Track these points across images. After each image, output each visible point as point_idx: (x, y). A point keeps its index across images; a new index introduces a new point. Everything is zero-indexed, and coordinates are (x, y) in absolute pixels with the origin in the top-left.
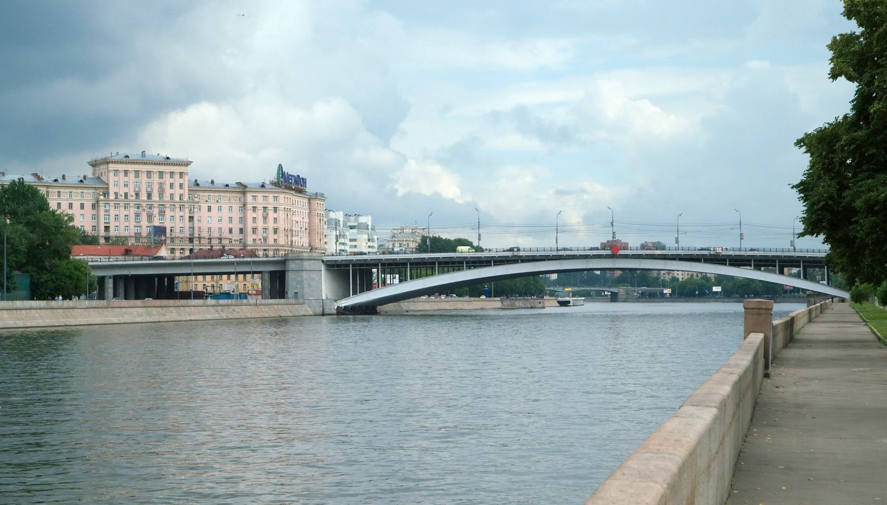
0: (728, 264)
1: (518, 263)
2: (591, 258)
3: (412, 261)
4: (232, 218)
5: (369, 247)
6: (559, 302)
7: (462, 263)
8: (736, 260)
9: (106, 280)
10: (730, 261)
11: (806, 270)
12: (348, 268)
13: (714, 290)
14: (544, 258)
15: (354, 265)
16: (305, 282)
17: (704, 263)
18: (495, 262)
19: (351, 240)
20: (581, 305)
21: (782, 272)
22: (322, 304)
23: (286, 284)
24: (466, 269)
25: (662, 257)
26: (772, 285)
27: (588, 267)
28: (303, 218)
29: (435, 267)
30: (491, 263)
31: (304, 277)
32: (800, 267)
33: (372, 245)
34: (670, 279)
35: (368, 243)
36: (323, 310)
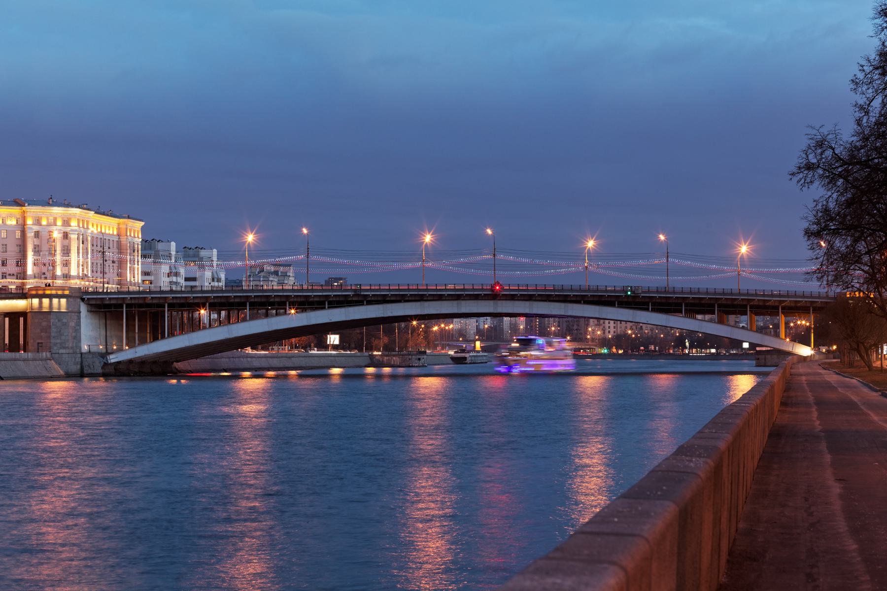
0: (650, 309)
1: (363, 305)
2: (482, 299)
4: (6, 245)
8: (661, 304)
10: (654, 304)
11: (3, 222)
13: (337, 337)
14: (398, 299)
15: (128, 306)
16: (53, 329)
17: (618, 307)
20: (482, 363)
21: (721, 321)
22: (80, 360)
25: (561, 299)
30: (325, 305)
31: (52, 321)
32: (714, 314)
35: (212, 284)
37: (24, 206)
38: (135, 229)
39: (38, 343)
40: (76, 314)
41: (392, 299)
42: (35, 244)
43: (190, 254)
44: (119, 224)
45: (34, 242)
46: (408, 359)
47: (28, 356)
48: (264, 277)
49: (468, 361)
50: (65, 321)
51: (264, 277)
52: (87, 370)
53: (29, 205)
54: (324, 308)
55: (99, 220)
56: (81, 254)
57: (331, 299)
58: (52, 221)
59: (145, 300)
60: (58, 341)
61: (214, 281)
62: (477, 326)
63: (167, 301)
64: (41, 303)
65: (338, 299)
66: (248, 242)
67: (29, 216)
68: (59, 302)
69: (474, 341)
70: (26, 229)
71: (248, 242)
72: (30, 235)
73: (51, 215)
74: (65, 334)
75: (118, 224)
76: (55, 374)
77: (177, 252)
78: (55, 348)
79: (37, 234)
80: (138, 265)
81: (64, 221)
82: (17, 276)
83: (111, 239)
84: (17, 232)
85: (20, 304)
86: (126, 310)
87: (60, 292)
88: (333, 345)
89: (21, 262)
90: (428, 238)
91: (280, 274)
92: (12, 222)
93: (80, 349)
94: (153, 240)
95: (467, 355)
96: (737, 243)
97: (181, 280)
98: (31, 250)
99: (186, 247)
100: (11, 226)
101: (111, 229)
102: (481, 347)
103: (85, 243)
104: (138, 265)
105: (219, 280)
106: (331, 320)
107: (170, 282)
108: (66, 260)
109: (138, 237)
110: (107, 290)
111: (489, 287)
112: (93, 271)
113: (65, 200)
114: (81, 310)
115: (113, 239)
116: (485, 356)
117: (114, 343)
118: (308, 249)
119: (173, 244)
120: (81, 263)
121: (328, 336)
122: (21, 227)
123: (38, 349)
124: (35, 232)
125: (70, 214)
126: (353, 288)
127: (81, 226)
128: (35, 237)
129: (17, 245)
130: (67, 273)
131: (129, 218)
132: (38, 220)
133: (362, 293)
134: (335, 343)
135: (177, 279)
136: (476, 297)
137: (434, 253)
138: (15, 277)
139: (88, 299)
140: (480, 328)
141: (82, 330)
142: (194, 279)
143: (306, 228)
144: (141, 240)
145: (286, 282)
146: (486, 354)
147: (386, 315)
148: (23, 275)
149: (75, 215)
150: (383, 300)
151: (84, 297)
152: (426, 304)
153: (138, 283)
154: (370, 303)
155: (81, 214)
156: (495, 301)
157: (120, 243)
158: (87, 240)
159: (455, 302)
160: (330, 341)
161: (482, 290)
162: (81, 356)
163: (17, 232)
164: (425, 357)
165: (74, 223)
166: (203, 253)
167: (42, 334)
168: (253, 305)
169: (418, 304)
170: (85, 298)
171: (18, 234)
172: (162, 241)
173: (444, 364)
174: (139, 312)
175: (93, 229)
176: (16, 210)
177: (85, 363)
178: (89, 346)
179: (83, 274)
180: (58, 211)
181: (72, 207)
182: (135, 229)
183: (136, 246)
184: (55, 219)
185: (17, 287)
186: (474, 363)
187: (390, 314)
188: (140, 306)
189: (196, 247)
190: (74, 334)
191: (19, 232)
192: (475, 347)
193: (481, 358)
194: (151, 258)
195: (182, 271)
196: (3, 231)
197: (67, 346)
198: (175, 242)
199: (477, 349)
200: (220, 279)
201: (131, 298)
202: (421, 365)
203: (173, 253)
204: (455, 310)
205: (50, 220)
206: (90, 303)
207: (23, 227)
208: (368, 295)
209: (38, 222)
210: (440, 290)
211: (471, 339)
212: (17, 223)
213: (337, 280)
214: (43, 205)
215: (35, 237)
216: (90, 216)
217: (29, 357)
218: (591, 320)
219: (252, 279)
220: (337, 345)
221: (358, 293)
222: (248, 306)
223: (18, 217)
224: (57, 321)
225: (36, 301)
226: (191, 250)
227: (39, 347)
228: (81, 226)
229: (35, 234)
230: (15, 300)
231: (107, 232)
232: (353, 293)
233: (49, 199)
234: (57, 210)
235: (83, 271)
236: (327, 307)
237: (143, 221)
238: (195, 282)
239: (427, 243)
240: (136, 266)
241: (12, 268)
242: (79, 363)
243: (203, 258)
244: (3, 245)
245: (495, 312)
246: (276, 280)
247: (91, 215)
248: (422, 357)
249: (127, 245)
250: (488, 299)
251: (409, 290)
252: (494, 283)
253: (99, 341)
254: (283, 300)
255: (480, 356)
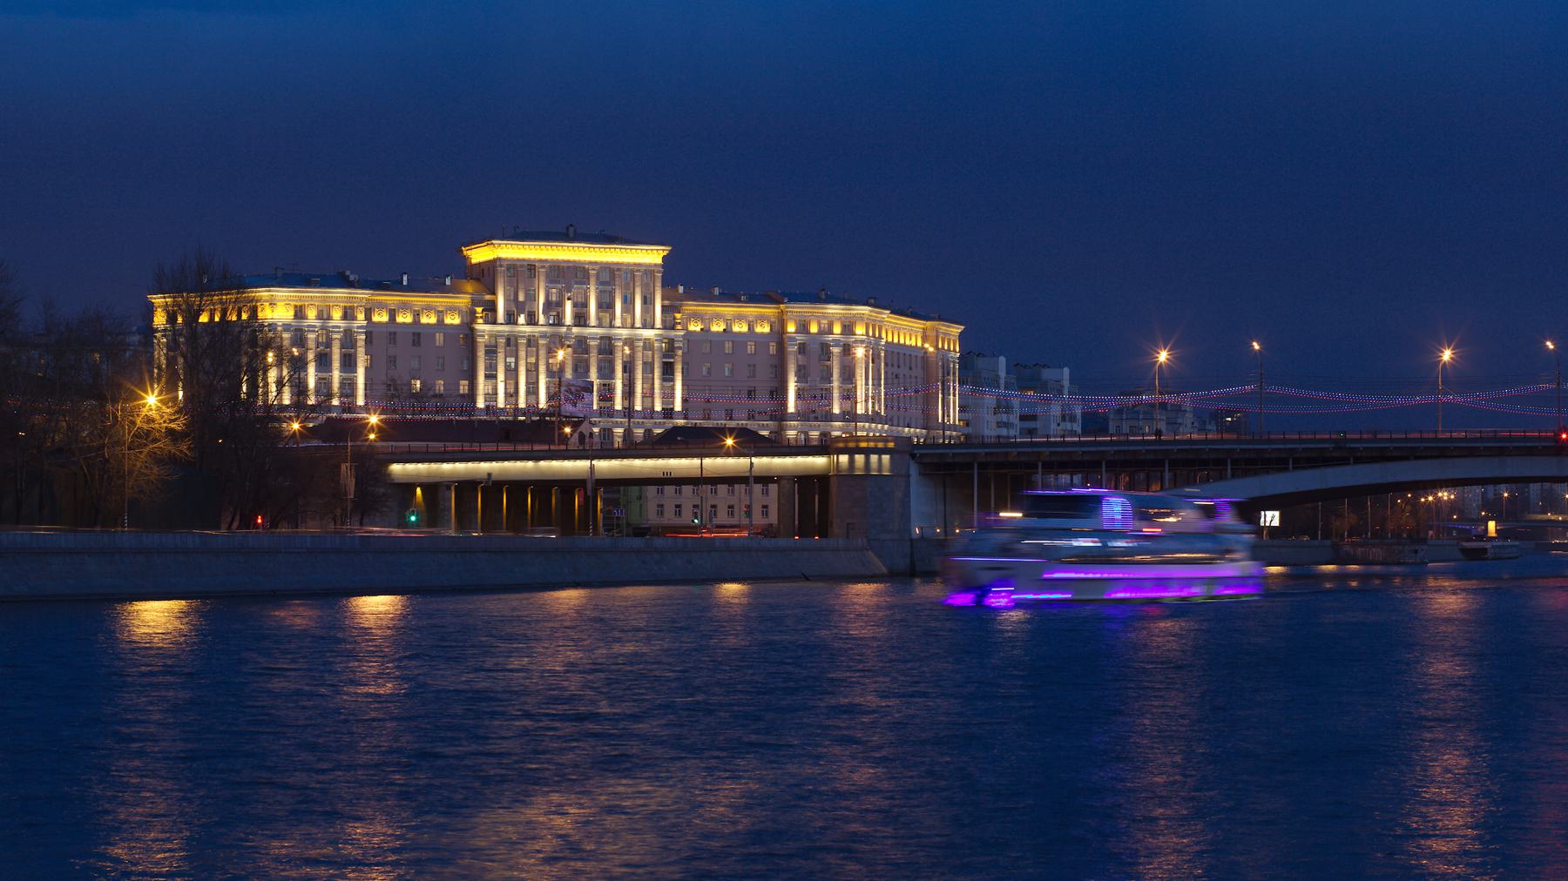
1: (1349, 464)
3: (1359, 454)
7: (1222, 462)
11: (749, 329)
15: (981, 466)
28: (911, 368)
29: (1227, 470)
33: (1005, 420)
34: (1412, 835)
35: (1062, 424)
38: (948, 338)
39: (848, 524)
42: (800, 363)
45: (797, 360)
46: (1396, 552)
48: (1144, 413)
49: (1489, 555)
51: (1144, 413)
54: (1286, 469)
55: (897, 324)
58: (826, 326)
64: (852, 461)
67: (791, 319)
68: (880, 459)
69: (1485, 521)
70: (786, 341)
73: (825, 318)
75: (923, 329)
77: (1008, 373)
80: (954, 395)
81: (845, 326)
84: (771, 344)
86: (978, 473)
87: (880, 445)
88: (1270, 526)
89: (780, 392)
91: (1169, 408)
93: (910, 535)
96: (1438, 346)
98: (793, 374)
101: (914, 339)
103: (876, 360)
114: (911, 473)
115: (898, 350)
116: (1515, 546)
121: (1263, 513)
123: (848, 533)
124: (800, 344)
126: (1334, 436)
127: (871, 334)
128: (800, 353)
129: (771, 366)
130: (849, 409)
131: (940, 319)
133: (1348, 446)
135: (1072, 426)
138: (768, 417)
139: (921, 454)
141: (912, 504)
142: (1033, 418)
145: (1180, 421)
146: (1517, 543)
148: (780, 416)
149: (861, 318)
150: (1382, 456)
151: (915, 452)
154: (1359, 460)
157: (927, 361)
163: (771, 344)
165: (860, 330)
166: (1047, 374)
171: (773, 349)
176: (769, 310)
179: (873, 411)
182: (948, 338)
184: (831, 325)
195: (1016, 402)
198: (1005, 356)
199: (1490, 535)
201: (986, 453)
204: (1497, 473)
205: (822, 325)
207: (779, 334)
208: (1387, 448)
209: (803, 328)
212: (771, 330)
215: (800, 353)
216: (884, 318)
222: (1167, 465)
223: (773, 320)
225: (844, 459)
228: (871, 334)
229: (799, 348)
231: (908, 343)
232: (1333, 446)
234: (834, 309)
235: (873, 407)
237: (961, 325)
238: (1034, 422)
241: (763, 402)
244: (749, 366)
246: (1164, 418)
249: (937, 364)
255: (1508, 547)
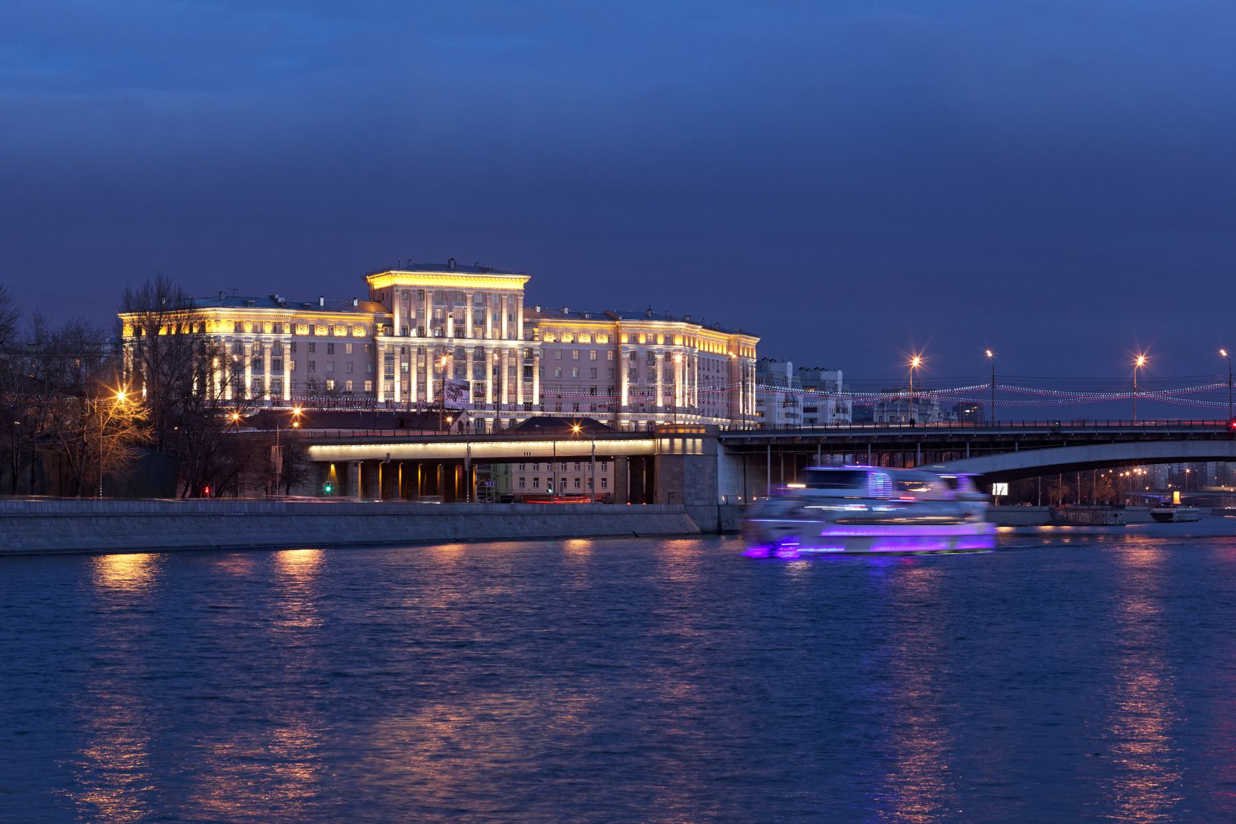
1: (1062, 446)
2: (1215, 440)
5: (788, 415)
6: (1155, 515)
9: (350, 468)
11: (592, 340)
12: (765, 452)
13: (1006, 485)
15: (774, 447)
18: (1021, 444)
19: (806, 410)
20: (1192, 521)
23: (655, 477)
24: (971, 456)
26: (521, 437)
27: (1211, 455)
28: (718, 371)
29: (966, 451)
30: (1015, 446)
31: (685, 466)
35: (837, 415)
36: (719, 524)
37: (618, 320)
39: (669, 493)
40: (713, 458)
41: (1099, 439)
43: (809, 378)
44: (729, 341)
45: (630, 365)
47: (661, 508)
49: (1175, 518)
50: (700, 466)
52: (725, 527)
53: (623, 318)
55: (707, 336)
56: (686, 382)
57: (1022, 439)
58: (652, 338)
59: (794, 440)
60: (693, 491)
61: (839, 412)
62: (1169, 469)
63: (820, 441)
64: (672, 444)
65: (1031, 439)
66: (913, 367)
67: (625, 333)
68: (694, 442)
69: (1171, 491)
70: (620, 349)
71: (913, 367)
72: (625, 356)
73: (651, 331)
74: (701, 482)
76: (691, 530)
77: (794, 375)
78: (689, 499)
79: (633, 356)
80: (752, 392)
82: (609, 408)
83: (720, 360)
84: (609, 352)
85: (646, 444)
86: (771, 453)
87: (694, 431)
89: (615, 389)
90: (1141, 361)
91: (921, 402)
92: (603, 340)
94: (764, 359)
95: (1173, 511)
97: (799, 411)
99: (802, 368)
100: (602, 344)
102: (1181, 499)
104: (752, 392)
105: (845, 411)
106: (1022, 465)
107: (786, 414)
108: (669, 388)
109: (752, 357)
110: (749, 428)
111: (1223, 423)
112: (699, 402)
113: (667, 312)
115: (717, 359)
116: (1196, 511)
117: (754, 493)
118: (993, 376)
119: (790, 364)
120: (687, 392)
121: (994, 485)
122: (613, 346)
125: (674, 330)
126: (1051, 425)
127: (687, 344)
128: (631, 359)
129: (609, 369)
131: (741, 332)
132: (634, 338)
133: (1062, 432)
134: (1002, 494)
135: (794, 410)
136: (1207, 437)
137: (1149, 380)
140: (1173, 474)
143: (990, 350)
144: (755, 361)
145: (929, 412)
146: (1197, 509)
147: (1092, 460)
148: (616, 408)
149: (679, 331)
150: (1088, 440)
151: (721, 437)
152: (1143, 445)
153: (753, 416)
154: (1071, 444)
155: (687, 330)
156: (1231, 442)
158: (693, 362)
159: (1180, 443)
160: (996, 491)
161: (1215, 426)
162: (719, 509)
163: (609, 352)
164: (1123, 512)
165: (678, 341)
166: (825, 376)
167: (674, 481)
168: (925, 446)
169: (1132, 445)
170: (722, 439)
171: (610, 356)
172: (775, 361)
173: (1137, 523)
174: (784, 454)
175: (700, 347)
176: (608, 326)
177: (723, 518)
178: (727, 496)
180: (662, 327)
181: (676, 320)
183: (750, 369)
184: (655, 337)
185: (609, 421)
186: (1182, 521)
187: (1097, 459)
188: (787, 447)
189: (800, 367)
190: (710, 482)
191: (611, 352)
192: (1172, 499)
193: (1189, 515)
194: (762, 384)
196: (591, 352)
197: (703, 496)
200: (847, 409)
202: (1118, 523)
203: (790, 375)
205: (649, 338)
206: (728, 444)
207: (615, 344)
209: (634, 339)
210: (1160, 428)
211: (1161, 488)
212: (609, 341)
213: (969, 406)
214: (641, 319)
216: (697, 332)
217: (663, 510)
218: (419, 365)
219: (886, 409)
220: (1005, 496)
221: (1056, 431)
223: (610, 333)
224: (691, 466)
225: (666, 442)
226: (809, 373)
227: (670, 498)
228: (687, 344)
229: (631, 355)
230: (640, 441)
231: (716, 351)
232: (1050, 432)
233: (648, 311)
234: (658, 325)
235: (689, 401)
236: (1017, 449)
239: (1139, 367)
240: (750, 394)
242: (716, 518)
243: (773, 374)
244: (592, 369)
245: (1231, 456)
246: (917, 410)
247: (698, 330)
248: (1120, 512)
249: (739, 368)
250: (1222, 440)
251: (1121, 427)
252: (1229, 419)
253: (737, 492)
254: (962, 440)
